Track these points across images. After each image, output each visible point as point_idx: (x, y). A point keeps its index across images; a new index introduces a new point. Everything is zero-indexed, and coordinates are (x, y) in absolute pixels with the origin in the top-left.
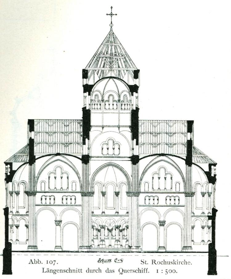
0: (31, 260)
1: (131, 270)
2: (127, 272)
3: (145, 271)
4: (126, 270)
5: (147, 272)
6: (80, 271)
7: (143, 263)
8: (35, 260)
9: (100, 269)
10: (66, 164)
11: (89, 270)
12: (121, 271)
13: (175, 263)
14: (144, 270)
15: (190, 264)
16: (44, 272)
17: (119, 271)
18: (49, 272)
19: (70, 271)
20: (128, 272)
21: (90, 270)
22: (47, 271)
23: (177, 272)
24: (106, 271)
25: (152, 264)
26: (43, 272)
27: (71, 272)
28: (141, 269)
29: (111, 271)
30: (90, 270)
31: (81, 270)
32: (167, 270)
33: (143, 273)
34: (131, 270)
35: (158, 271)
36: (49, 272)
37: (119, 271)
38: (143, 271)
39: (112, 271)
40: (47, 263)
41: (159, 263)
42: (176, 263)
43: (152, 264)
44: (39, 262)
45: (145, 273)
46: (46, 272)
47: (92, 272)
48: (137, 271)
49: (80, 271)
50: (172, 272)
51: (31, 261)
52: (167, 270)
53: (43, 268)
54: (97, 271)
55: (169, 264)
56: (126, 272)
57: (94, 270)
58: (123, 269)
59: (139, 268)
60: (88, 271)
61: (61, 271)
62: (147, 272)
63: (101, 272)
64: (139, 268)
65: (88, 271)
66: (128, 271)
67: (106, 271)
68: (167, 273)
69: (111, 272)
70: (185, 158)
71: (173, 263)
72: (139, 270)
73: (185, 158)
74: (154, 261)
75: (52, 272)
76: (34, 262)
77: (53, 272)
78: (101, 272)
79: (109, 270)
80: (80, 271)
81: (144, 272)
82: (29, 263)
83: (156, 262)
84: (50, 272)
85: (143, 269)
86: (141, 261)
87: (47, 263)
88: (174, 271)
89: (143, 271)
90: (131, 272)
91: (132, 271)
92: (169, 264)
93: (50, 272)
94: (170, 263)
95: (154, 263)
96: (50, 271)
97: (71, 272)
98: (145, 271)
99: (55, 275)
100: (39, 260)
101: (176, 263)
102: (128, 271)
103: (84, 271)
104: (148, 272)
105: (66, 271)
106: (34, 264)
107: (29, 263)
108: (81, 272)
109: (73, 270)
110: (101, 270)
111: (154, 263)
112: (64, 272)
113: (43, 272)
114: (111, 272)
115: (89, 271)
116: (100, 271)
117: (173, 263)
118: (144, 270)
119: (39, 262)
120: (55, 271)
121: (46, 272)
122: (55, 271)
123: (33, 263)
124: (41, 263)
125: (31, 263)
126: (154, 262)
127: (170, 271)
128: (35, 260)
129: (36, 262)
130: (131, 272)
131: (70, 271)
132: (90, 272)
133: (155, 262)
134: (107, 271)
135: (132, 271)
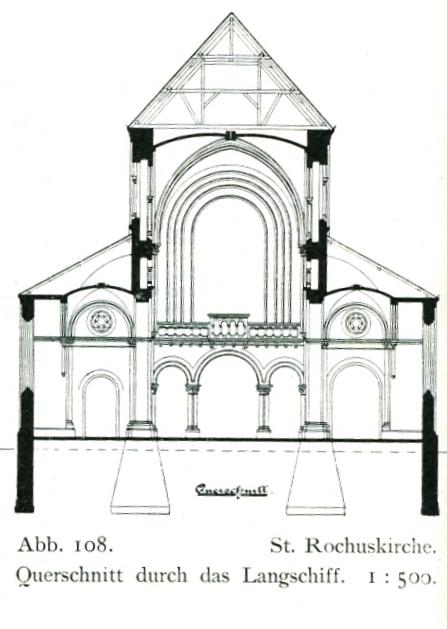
0: (26, 539)
1: (56, 574)
2: (43, 578)
3: (332, 577)
4: (40, 573)
5: (336, 581)
6: (115, 576)
7: (277, 549)
8: (37, 538)
9: (84, 570)
10: (196, 227)
11: (144, 573)
12: (24, 574)
13: (381, 550)
14: (329, 573)
15: (432, 550)
16: (249, 580)
17: (18, 575)
18: (264, 581)
19: (84, 576)
20: (48, 578)
21: (150, 574)
22: (257, 578)
23: (434, 583)
24: (138, 577)
25: (309, 551)
26: (246, 581)
27: (316, 581)
28: (318, 572)
29: (218, 577)
30: (150, 574)
31: (119, 573)
32: (403, 573)
33: (325, 584)
34: (56, 574)
35: (370, 580)
36: (264, 581)
37: (18, 575)
38: (325, 579)
39: (221, 578)
40: (78, 550)
41: (329, 548)
42: (387, 548)
43: (309, 551)
44: (53, 547)
45: (332, 584)
46: (255, 581)
47: (156, 580)
48: (75, 577)
49: (182, 576)
50: (420, 582)
51: (25, 543)
52: (403, 573)
53: (246, 569)
54: (172, 577)
55: (364, 551)
56: (40, 580)
57: (162, 574)
58: (32, 571)
59: (81, 568)
60: (205, 577)
61: (273, 577)
62: (336, 581)
63: (185, 581)
64: (81, 568)
65: (141, 577)
66: (45, 575)
67: (138, 577)
68: (402, 582)
69: (219, 581)
70: (305, 144)
71: (376, 547)
72: (82, 574)
73: (305, 144)
74: (313, 542)
75: (276, 581)
76: (33, 547)
77: (279, 579)
78: (185, 581)
79: (211, 573)
80: (115, 576)
81: (329, 581)
82: (20, 550)
83: (320, 546)
84: (270, 581)
85: (325, 572)
86: (273, 544)
87: (78, 550)
88: (426, 578)
89: (325, 579)
90: (56, 580)
91: (60, 577)
92: (364, 551)
93: (364, 545)
94: (367, 549)
95: (312, 548)
96: (267, 578)
97: (316, 581)
98: (332, 577)
99: (284, 590)
100: (40, 540)
101: (387, 548)
102: (45, 575)
103: (129, 576)
104: (339, 578)
105: (69, 576)
106: (36, 552)
107: (20, 550)
108: (119, 581)
109: (93, 573)
110: (184, 574)
111: (312, 548)
112: (371, 550)
113: (246, 581)
114: (219, 581)
115: (144, 576)
116: (182, 576)
117: (376, 549)
118: (329, 573)
119: (53, 547)
120: (283, 576)
121: (255, 581)
122: (283, 576)
123: (30, 550)
124: (58, 548)
125: (26, 548)
126: (315, 546)
127: (414, 578)
128: (37, 538)
129: (41, 546)
130: (56, 580)
131: (84, 576)
132: (151, 580)
133: (318, 546)
134: (205, 577)
135: (60, 577)
